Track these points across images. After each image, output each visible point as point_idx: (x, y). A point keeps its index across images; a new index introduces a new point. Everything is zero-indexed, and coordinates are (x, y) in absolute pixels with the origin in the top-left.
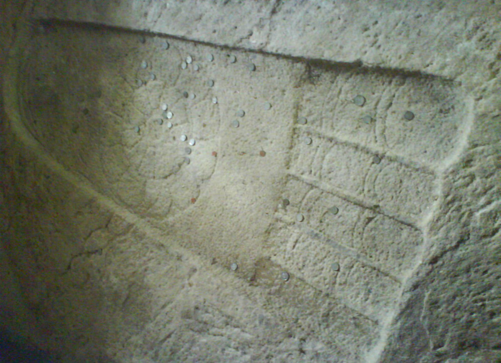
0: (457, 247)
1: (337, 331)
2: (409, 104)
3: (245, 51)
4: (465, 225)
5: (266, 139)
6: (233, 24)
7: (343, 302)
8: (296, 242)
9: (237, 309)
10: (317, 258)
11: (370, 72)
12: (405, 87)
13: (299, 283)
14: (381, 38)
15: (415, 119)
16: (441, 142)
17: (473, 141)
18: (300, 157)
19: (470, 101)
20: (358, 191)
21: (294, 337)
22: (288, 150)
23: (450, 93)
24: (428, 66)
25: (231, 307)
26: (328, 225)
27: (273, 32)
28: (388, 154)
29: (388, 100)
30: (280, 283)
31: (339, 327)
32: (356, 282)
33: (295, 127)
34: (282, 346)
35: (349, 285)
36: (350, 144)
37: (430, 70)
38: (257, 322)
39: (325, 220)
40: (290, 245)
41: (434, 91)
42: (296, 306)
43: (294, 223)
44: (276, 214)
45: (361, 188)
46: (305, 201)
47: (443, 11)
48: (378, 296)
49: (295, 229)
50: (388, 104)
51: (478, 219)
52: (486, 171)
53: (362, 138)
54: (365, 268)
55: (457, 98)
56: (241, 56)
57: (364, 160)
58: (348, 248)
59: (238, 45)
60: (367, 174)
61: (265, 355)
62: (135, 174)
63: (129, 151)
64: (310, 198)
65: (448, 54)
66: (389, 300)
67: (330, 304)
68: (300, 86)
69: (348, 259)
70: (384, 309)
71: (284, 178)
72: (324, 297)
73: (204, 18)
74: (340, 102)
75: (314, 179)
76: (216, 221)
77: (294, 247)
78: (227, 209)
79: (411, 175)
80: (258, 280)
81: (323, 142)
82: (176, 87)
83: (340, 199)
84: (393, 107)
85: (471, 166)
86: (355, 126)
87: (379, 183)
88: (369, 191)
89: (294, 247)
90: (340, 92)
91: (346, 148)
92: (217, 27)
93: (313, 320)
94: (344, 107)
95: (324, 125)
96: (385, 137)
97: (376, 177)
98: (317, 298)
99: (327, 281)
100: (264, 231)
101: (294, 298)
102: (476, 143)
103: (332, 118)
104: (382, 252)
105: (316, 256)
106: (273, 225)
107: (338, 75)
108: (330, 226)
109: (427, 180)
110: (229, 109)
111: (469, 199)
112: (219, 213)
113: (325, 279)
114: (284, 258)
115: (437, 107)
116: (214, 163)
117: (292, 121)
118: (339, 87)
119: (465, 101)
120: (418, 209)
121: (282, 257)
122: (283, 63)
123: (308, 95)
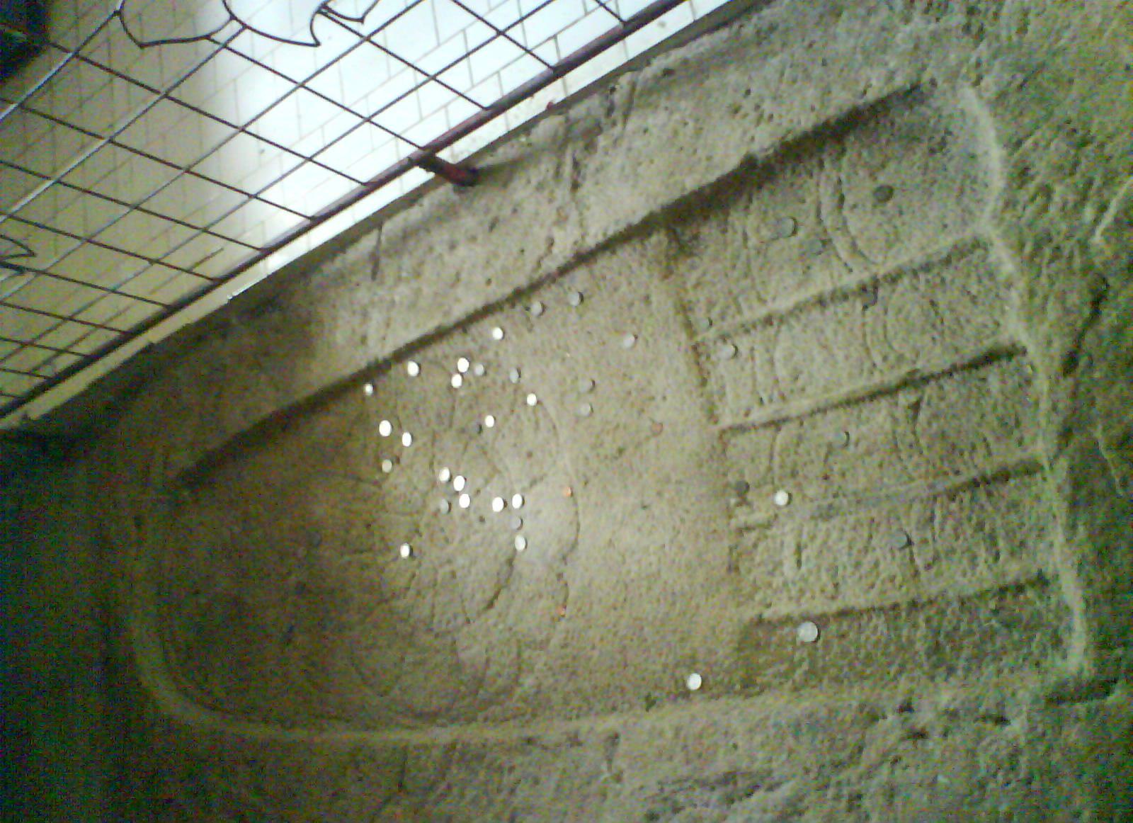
0: (1096, 312)
1: (974, 667)
2: (873, 176)
3: (554, 281)
4: (1088, 268)
5: (653, 398)
6: (515, 250)
7: (951, 594)
8: (799, 549)
9: (735, 746)
10: (855, 551)
11: (778, 166)
12: (850, 154)
13: (845, 624)
14: (767, 107)
15: (896, 192)
16: (962, 191)
17: (1010, 141)
18: (728, 389)
19: (968, 92)
20: (865, 374)
21: (884, 717)
22: (700, 391)
23: (929, 112)
24: (865, 92)
25: (721, 752)
26: (843, 475)
27: (586, 213)
28: (882, 272)
29: (834, 194)
30: (805, 655)
31: (975, 657)
32: (957, 538)
33: (693, 343)
34: (870, 755)
35: (947, 555)
36: (806, 302)
37: (871, 96)
38: (790, 741)
39: (832, 470)
40: (788, 568)
41: (900, 129)
42: (862, 677)
43: (776, 516)
44: (733, 521)
45: (867, 365)
46: (777, 460)
47: (845, 15)
48: (1014, 533)
49: (784, 525)
50: (836, 201)
51: (1103, 245)
52: (1061, 167)
53: (822, 282)
54: (958, 499)
55: (945, 113)
56: (548, 294)
57: (846, 314)
58: (902, 489)
59: (536, 276)
60: (864, 335)
61: (843, 804)
62: (426, 639)
63: (400, 604)
64: (785, 449)
65: (887, 58)
66: (1042, 523)
67: (928, 620)
68: (671, 272)
69: (917, 507)
70: (1041, 546)
71: (715, 444)
72: (908, 615)
73: (464, 276)
74: (753, 252)
75: (774, 407)
76: (621, 616)
77: (799, 562)
78: (633, 581)
79: (943, 280)
80: (759, 680)
81: (758, 335)
82: (455, 427)
83: (841, 411)
84: (849, 200)
85: (1032, 178)
86: (800, 271)
87: (896, 333)
88: (885, 359)
89: (799, 562)
90: (745, 237)
91: (803, 317)
92: (490, 273)
93: (912, 680)
94: (765, 256)
95: (744, 306)
96: (862, 255)
97: (885, 328)
98: (896, 629)
99: (899, 579)
100: (723, 570)
101: (851, 665)
102: (1014, 140)
103: (753, 287)
104: (973, 448)
105: (850, 548)
106: (736, 546)
107: (728, 214)
108: (848, 475)
109: (976, 266)
110: (563, 394)
111: (1064, 227)
112: (621, 599)
113: (892, 579)
114: (790, 598)
115: (921, 150)
116: (573, 510)
117: (683, 337)
118: (740, 231)
119: (960, 106)
120: (991, 325)
121: (785, 600)
122: (626, 254)
123: (693, 277)
